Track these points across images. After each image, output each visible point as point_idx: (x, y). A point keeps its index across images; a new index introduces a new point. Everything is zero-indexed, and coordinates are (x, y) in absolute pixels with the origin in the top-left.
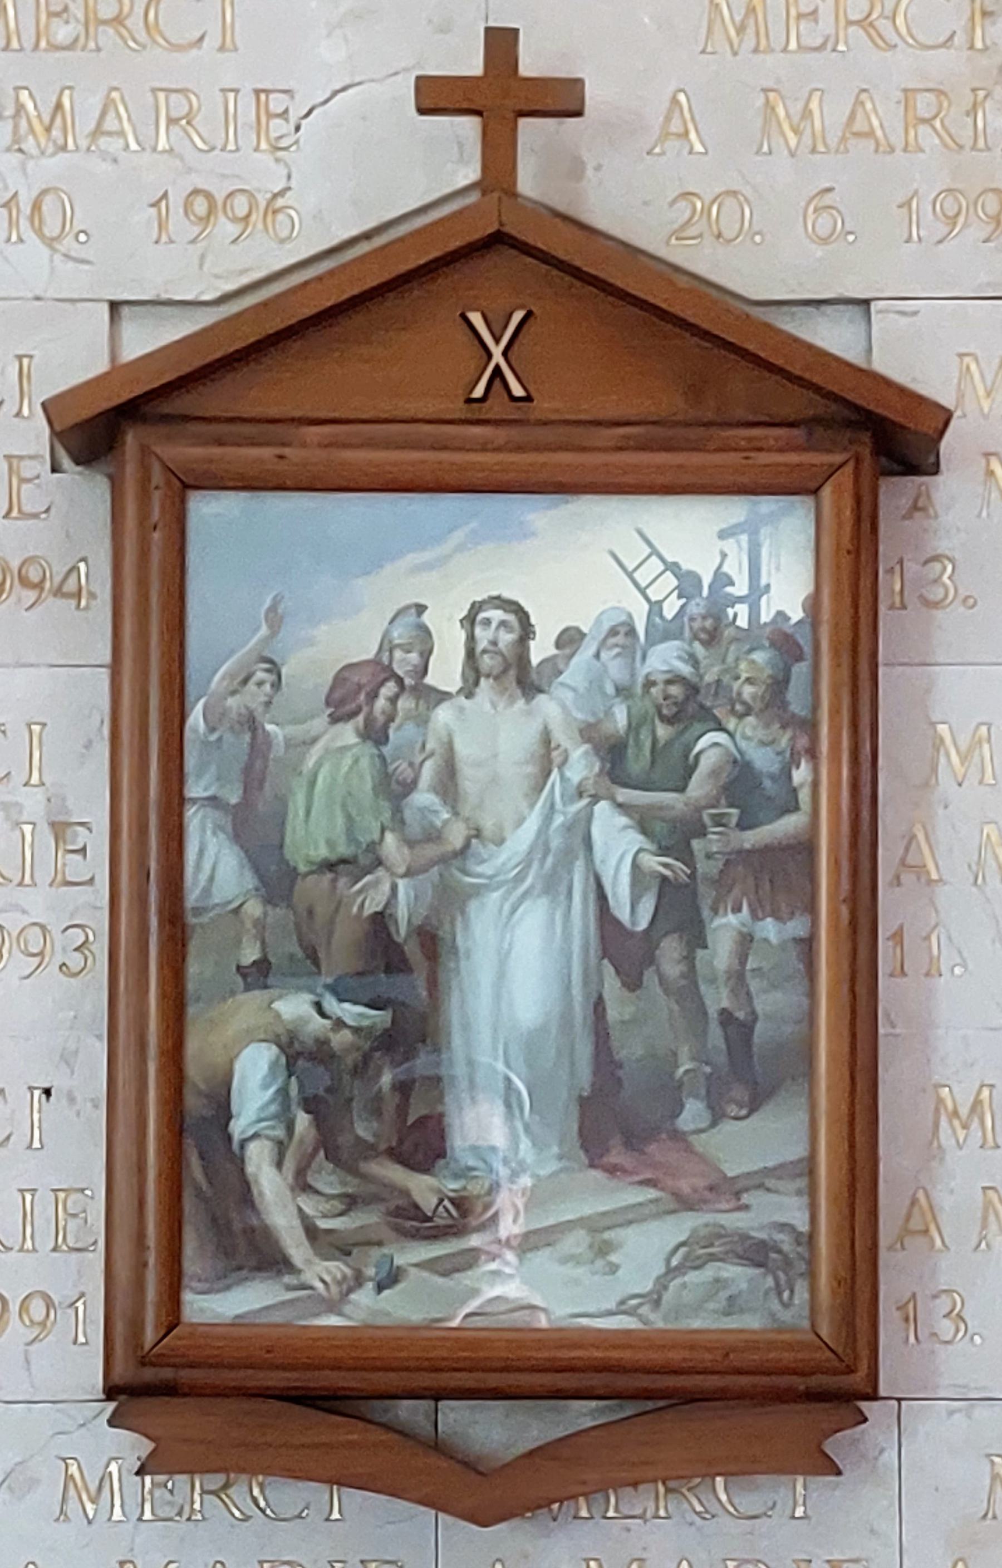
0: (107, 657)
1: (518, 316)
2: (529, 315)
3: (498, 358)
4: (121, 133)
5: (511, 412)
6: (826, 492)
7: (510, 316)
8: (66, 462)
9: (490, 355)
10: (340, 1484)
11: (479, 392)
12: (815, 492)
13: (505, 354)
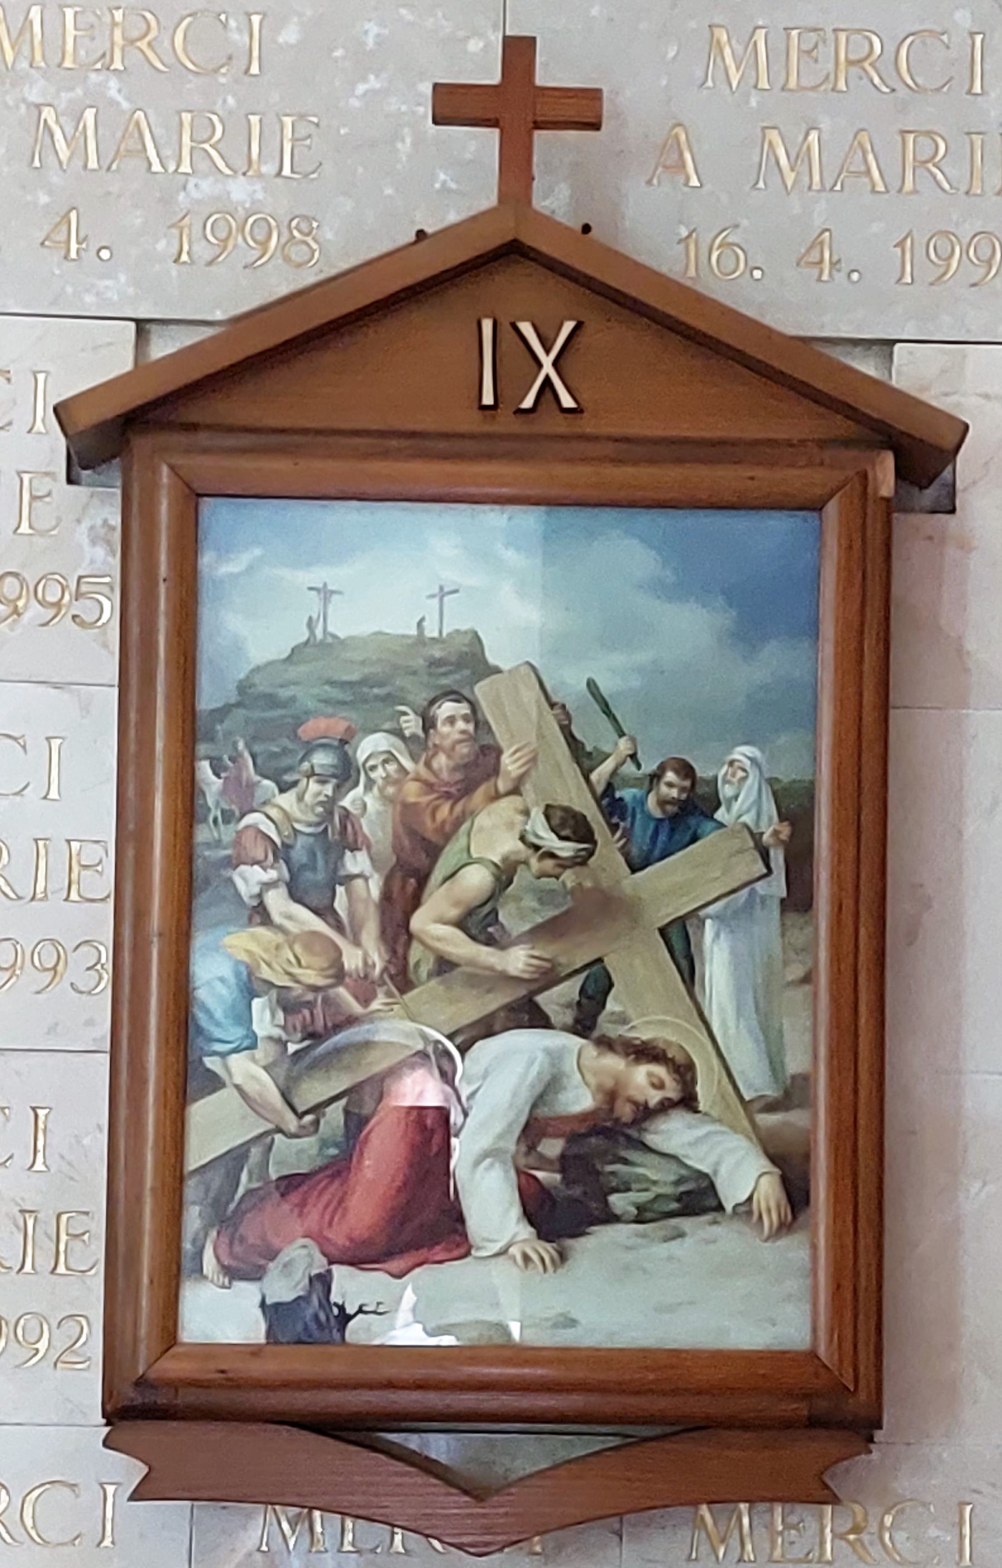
3: (548, 368)
5: (561, 426)
6: (832, 508)
9: (540, 365)
12: (817, 507)
13: (555, 364)
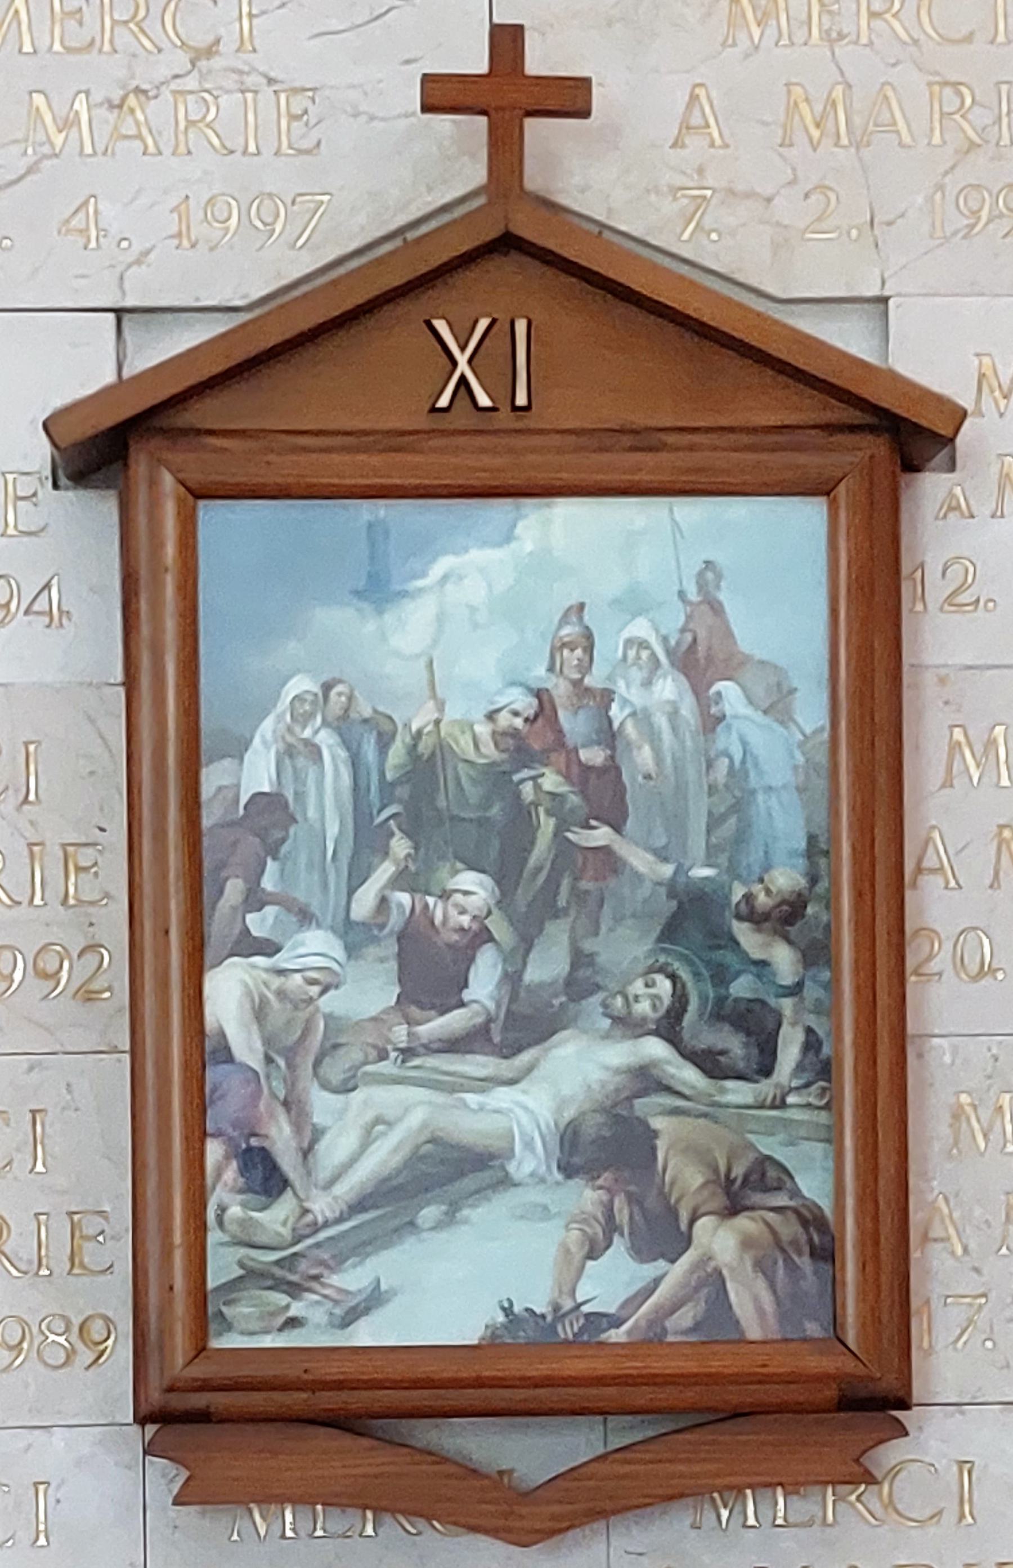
0: (119, 676)
1: (483, 324)
2: (494, 321)
4: (139, 137)
7: (476, 322)
8: (63, 481)
9: (454, 364)
10: (833, 1483)
11: (443, 402)
13: (470, 361)
